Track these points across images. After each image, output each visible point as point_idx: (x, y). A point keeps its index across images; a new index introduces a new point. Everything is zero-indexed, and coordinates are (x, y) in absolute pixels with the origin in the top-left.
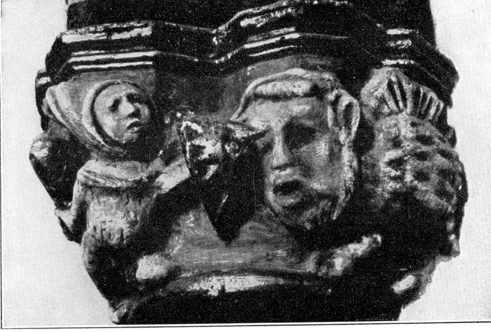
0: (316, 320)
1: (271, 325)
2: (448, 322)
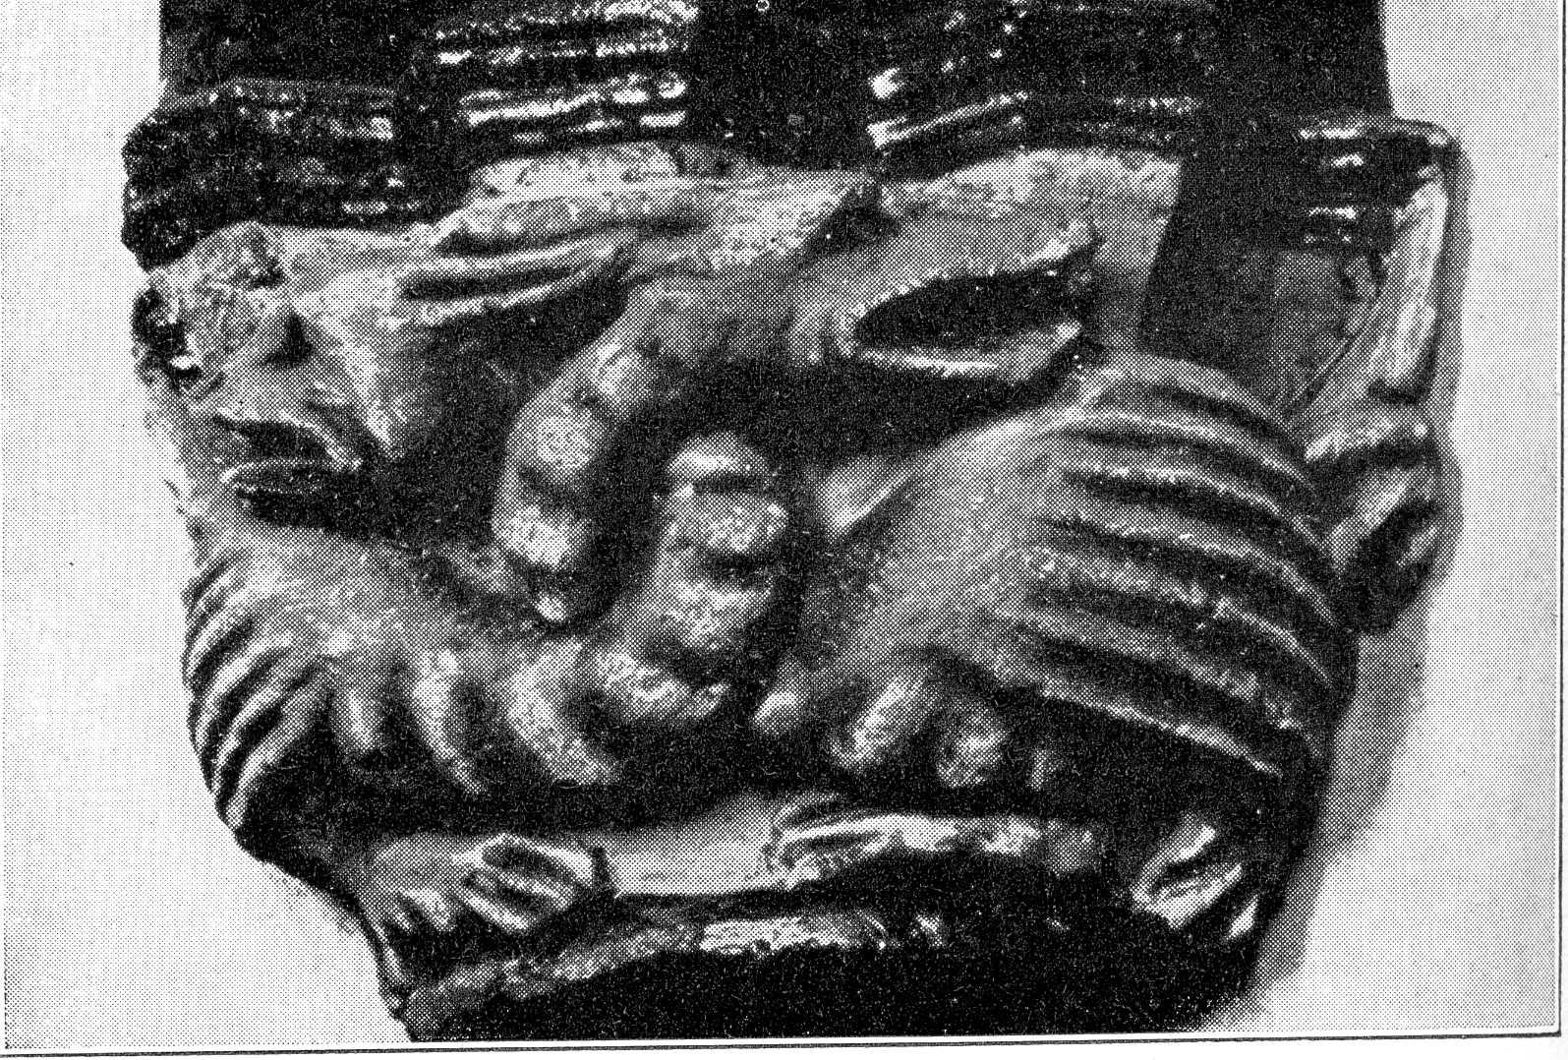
0: (656, 1032)
1: (832, 1045)
2: (111, 1052)
